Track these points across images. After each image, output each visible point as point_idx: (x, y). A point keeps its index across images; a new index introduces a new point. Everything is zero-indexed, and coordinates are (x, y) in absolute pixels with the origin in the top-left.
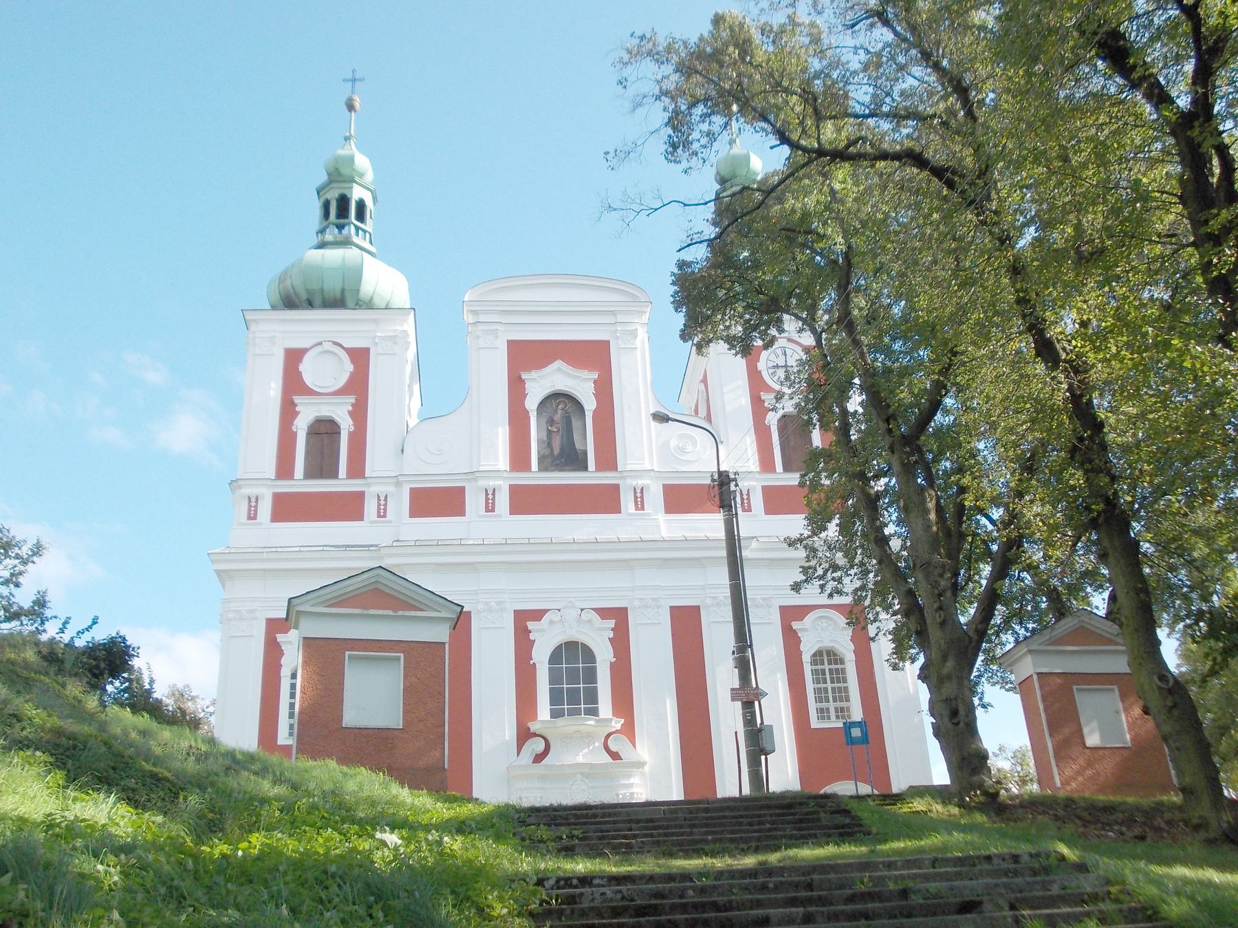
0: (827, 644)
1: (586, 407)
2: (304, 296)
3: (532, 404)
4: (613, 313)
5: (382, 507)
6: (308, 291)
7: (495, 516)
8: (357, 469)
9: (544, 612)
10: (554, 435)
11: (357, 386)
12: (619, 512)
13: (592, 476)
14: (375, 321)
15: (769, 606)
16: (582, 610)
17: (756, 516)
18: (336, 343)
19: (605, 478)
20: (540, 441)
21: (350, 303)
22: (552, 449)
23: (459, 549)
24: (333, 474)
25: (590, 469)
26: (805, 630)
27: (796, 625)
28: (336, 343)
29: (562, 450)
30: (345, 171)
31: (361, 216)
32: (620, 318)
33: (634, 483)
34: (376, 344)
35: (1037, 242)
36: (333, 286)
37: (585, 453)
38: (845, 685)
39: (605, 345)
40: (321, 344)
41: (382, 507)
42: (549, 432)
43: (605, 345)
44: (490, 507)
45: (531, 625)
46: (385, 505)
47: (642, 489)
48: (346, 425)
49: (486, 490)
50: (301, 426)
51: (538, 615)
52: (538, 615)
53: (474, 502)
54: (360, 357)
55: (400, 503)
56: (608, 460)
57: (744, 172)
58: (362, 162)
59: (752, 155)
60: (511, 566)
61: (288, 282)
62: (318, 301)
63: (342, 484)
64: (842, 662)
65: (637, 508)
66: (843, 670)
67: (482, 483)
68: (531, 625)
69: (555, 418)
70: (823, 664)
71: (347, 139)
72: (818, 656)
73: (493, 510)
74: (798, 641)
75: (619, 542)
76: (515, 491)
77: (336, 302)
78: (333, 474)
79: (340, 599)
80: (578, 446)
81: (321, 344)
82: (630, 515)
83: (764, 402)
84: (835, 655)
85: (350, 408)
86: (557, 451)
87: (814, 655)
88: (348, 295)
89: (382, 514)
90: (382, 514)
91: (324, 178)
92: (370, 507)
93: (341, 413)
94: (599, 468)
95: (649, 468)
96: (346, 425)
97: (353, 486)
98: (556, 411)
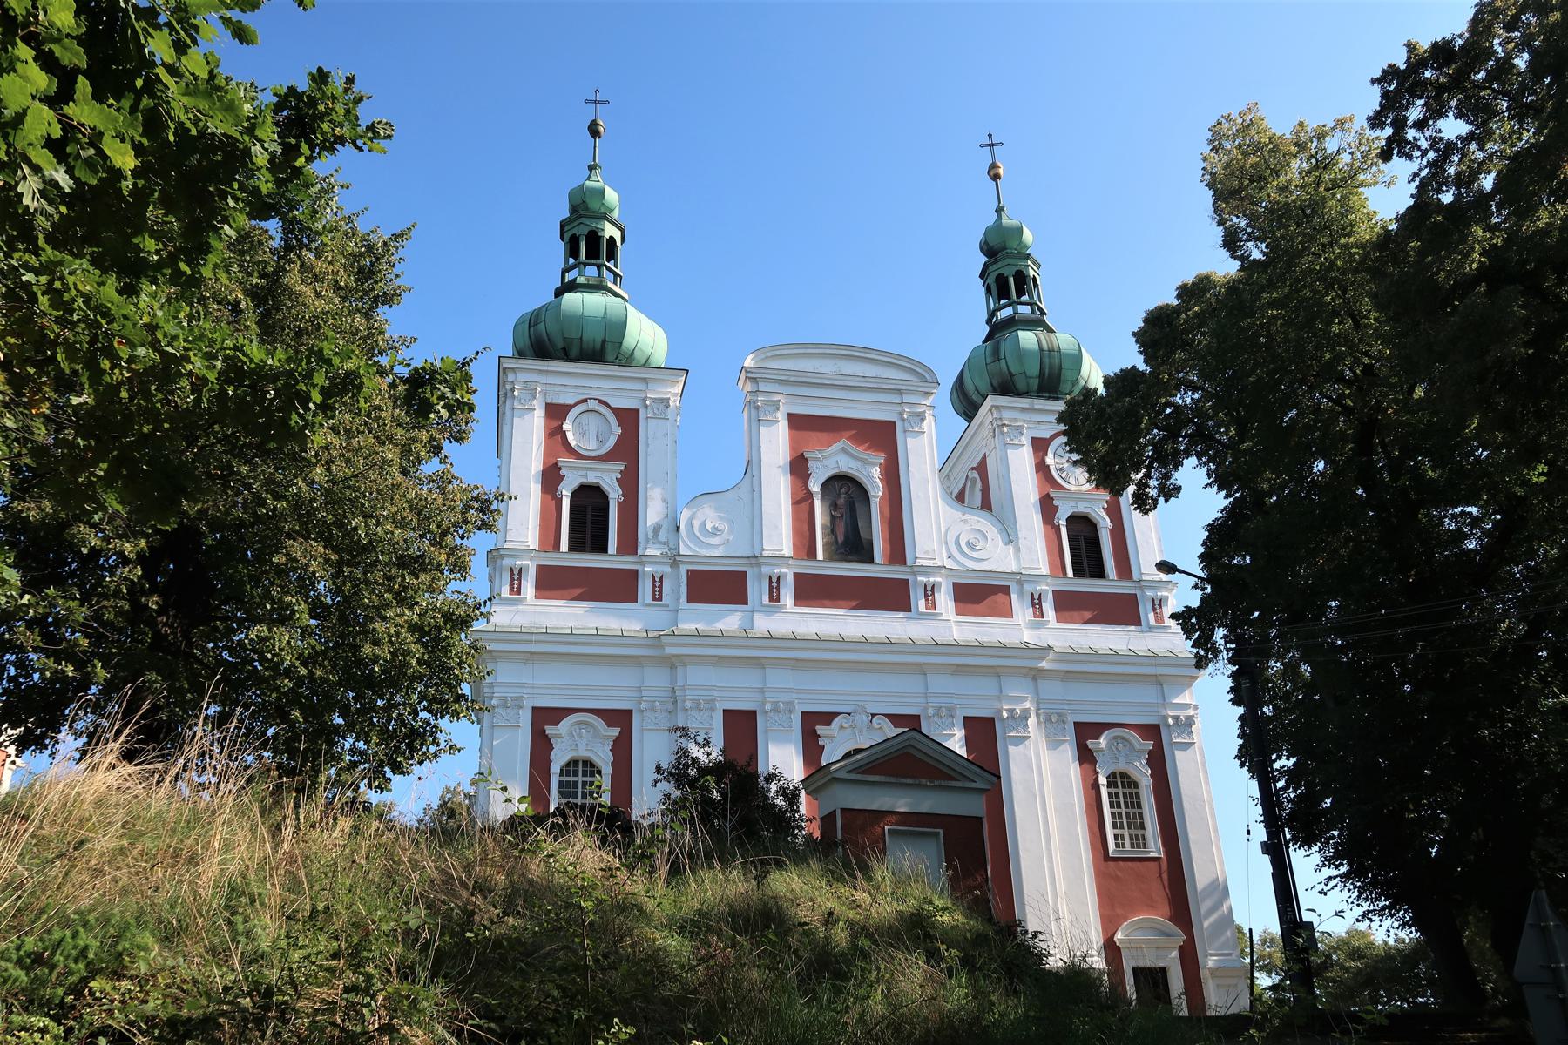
0: (583, 753)
1: (872, 493)
2: (560, 344)
3: (815, 487)
4: (899, 392)
5: (657, 589)
6: (565, 339)
7: (660, 605)
8: (629, 544)
9: (836, 714)
10: (838, 521)
11: (627, 451)
12: (635, 601)
13: (880, 568)
14: (645, 380)
15: (713, 709)
16: (873, 715)
17: (667, 606)
19: (895, 573)
20: (824, 527)
21: (610, 357)
22: (836, 537)
23: (742, 642)
24: (602, 548)
25: (609, 552)
26: (559, 736)
27: (549, 730)
28: (600, 401)
29: (847, 538)
30: (594, 205)
31: (612, 255)
32: (907, 399)
33: (925, 580)
34: (646, 407)
35: (1343, 353)
36: (593, 336)
37: (871, 543)
38: (1113, 810)
39: (891, 426)
42: (833, 518)
43: (891, 426)
44: (774, 597)
45: (820, 730)
46: (661, 587)
47: (779, 578)
48: (615, 494)
51: (828, 718)
52: (828, 718)
53: (757, 590)
54: (629, 419)
55: (676, 587)
56: (898, 553)
57: (1015, 245)
58: (611, 196)
59: (1025, 228)
60: (721, 661)
61: (542, 326)
62: (574, 351)
63: (612, 560)
64: (1136, 785)
65: (771, 599)
66: (1138, 795)
67: (766, 570)
68: (820, 730)
69: (838, 503)
70: (576, 774)
71: (592, 168)
72: (571, 767)
73: (519, 592)
74: (549, 747)
75: (723, 636)
76: (542, 571)
77: (595, 354)
78: (602, 548)
80: (863, 534)
82: (922, 614)
83: (1052, 499)
84: (1129, 777)
85: (619, 476)
86: (841, 539)
87: (568, 764)
88: (609, 347)
89: (657, 596)
90: (657, 596)
91: (565, 213)
92: (644, 589)
93: (608, 479)
94: (621, 550)
95: (940, 564)
97: (625, 563)
98: (839, 496)
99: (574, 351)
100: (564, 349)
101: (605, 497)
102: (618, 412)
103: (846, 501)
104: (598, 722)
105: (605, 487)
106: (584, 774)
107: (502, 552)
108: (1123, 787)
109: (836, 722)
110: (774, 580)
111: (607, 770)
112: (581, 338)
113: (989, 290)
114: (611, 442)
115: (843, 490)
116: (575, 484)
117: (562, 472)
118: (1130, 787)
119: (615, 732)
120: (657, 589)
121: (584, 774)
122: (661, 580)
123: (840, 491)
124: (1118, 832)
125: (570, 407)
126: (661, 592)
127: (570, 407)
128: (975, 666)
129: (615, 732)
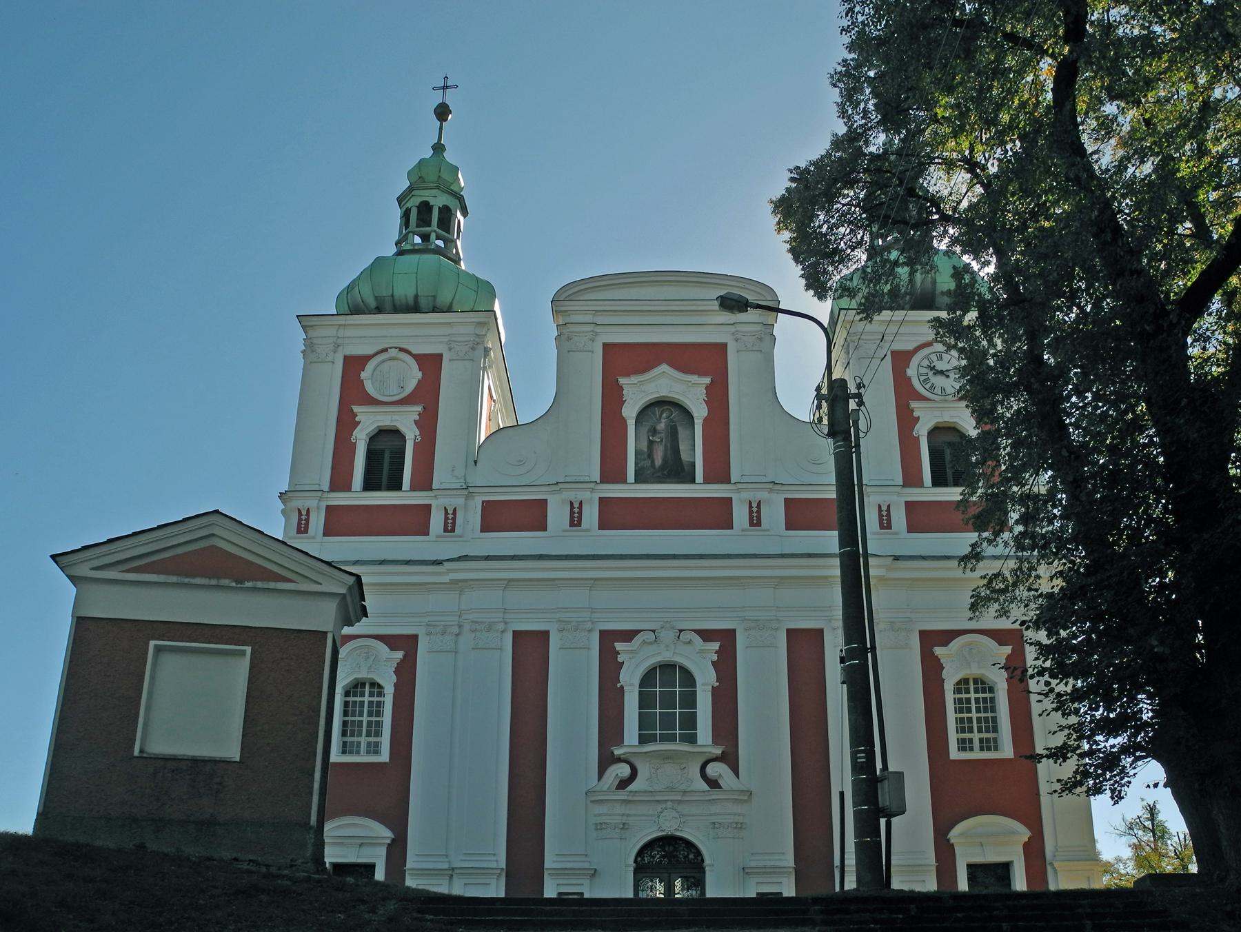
8: (424, 482)
9: (637, 632)
10: (656, 446)
16: (681, 631)
18: (402, 350)
27: (938, 651)
28: (402, 350)
29: (665, 461)
37: (693, 465)
40: (385, 350)
41: (576, 515)
45: (619, 646)
48: (411, 434)
49: (572, 504)
50: (922, 431)
54: (430, 364)
62: (388, 305)
63: (405, 497)
70: (968, 691)
72: (357, 687)
78: (396, 485)
79: (272, 585)
81: (385, 350)
84: (983, 683)
85: (417, 418)
87: (959, 683)
89: (450, 527)
92: (740, 515)
93: (406, 422)
96: (411, 434)
97: (419, 498)
99: (388, 305)
100: (377, 308)
101: (403, 438)
102: (419, 358)
103: (667, 426)
104: (382, 648)
105: (403, 429)
106: (371, 694)
107: (471, 490)
108: (976, 691)
109: (638, 640)
110: (754, 505)
111: (389, 690)
112: (392, 296)
113: (406, 216)
114: (411, 386)
115: (664, 415)
116: (930, 425)
117: (916, 414)
118: (984, 691)
119: (399, 655)
120: (450, 521)
121: (371, 694)
122: (889, 509)
123: (660, 416)
124: (976, 744)
125: (369, 358)
126: (759, 517)
127: (369, 358)
128: (441, 583)
129: (399, 655)
